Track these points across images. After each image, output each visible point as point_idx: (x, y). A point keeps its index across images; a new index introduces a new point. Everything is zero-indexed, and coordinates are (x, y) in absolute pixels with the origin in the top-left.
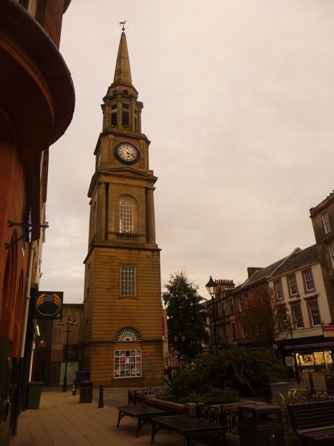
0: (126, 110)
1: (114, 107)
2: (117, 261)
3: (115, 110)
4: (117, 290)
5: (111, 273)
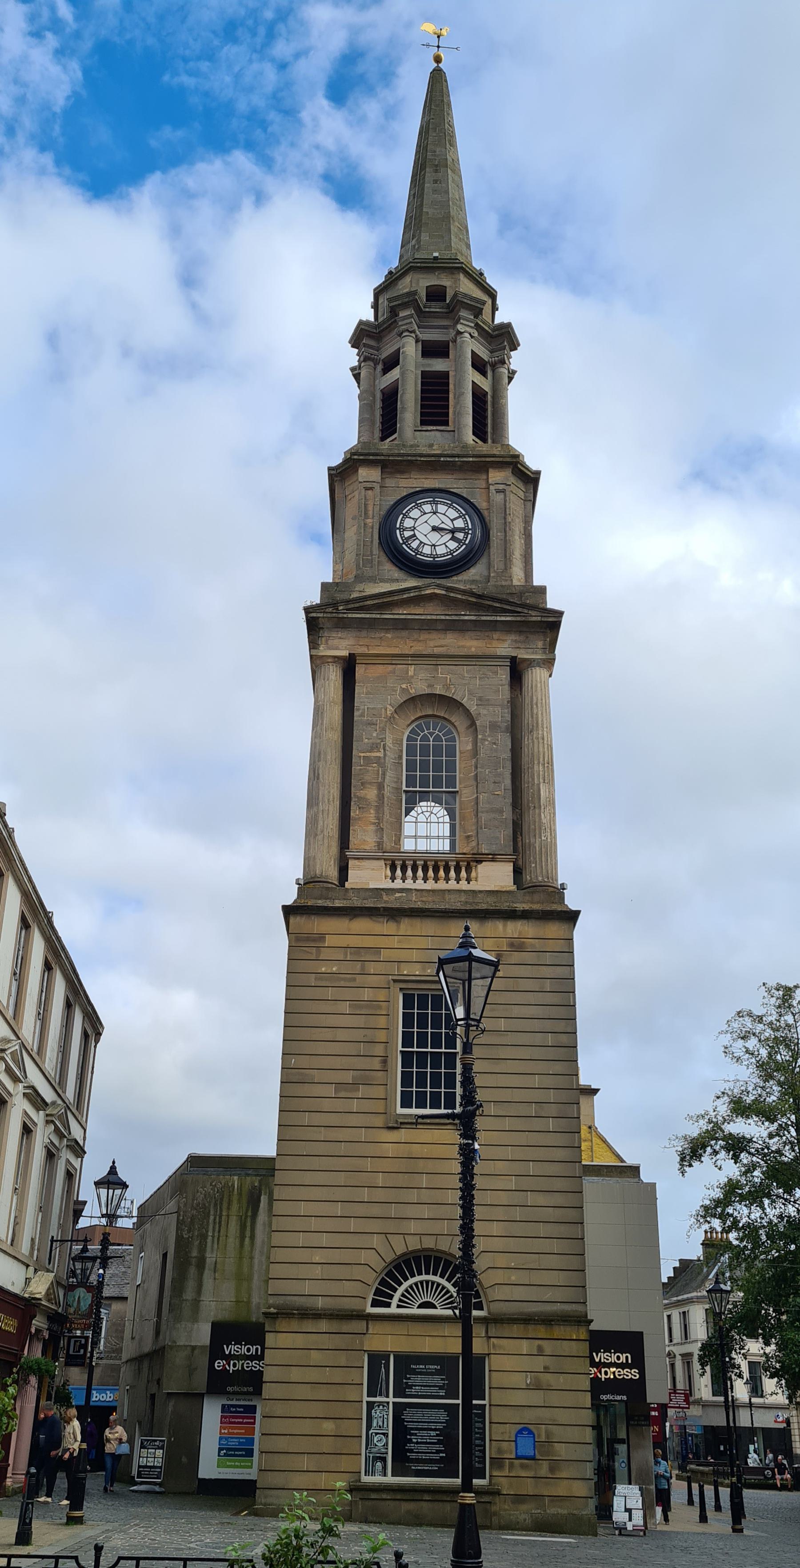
0: (438, 365)
1: (392, 362)
2: (380, 968)
3: (395, 373)
4: (382, 1022)
5: (359, 1021)
